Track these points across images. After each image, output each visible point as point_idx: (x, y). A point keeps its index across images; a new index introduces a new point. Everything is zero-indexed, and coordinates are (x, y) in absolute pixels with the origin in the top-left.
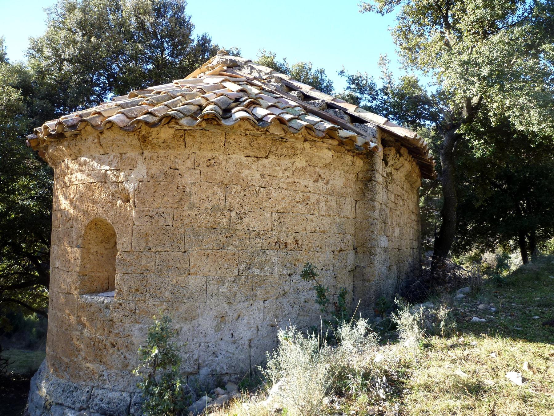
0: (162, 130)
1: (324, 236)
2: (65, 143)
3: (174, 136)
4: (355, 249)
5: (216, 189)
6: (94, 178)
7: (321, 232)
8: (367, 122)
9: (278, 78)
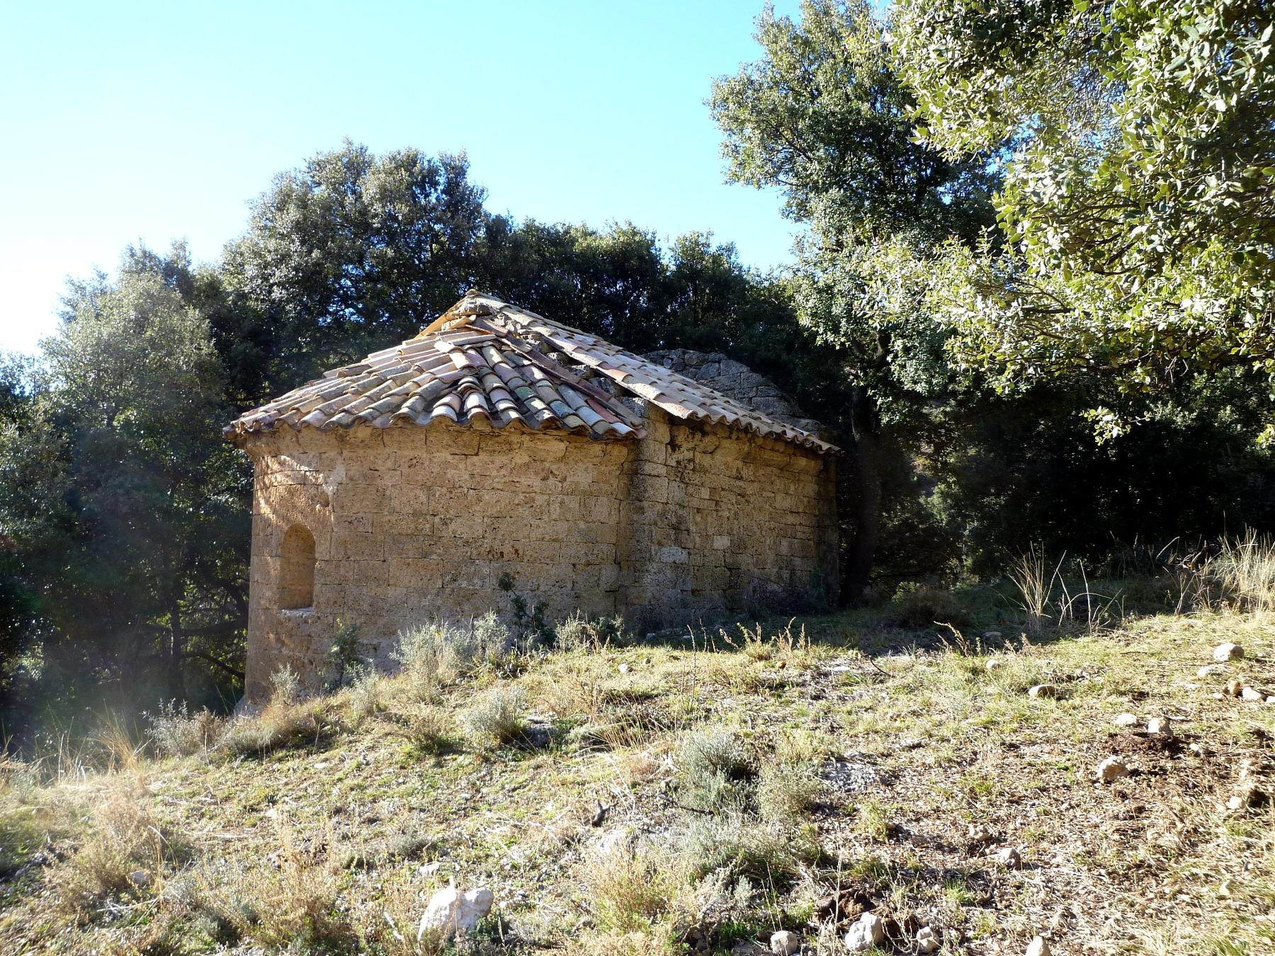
0: (360, 429)
1: (557, 545)
2: (264, 439)
3: (372, 435)
4: (618, 563)
5: (418, 492)
6: (293, 480)
7: (554, 540)
8: (636, 396)
9: (537, 333)
